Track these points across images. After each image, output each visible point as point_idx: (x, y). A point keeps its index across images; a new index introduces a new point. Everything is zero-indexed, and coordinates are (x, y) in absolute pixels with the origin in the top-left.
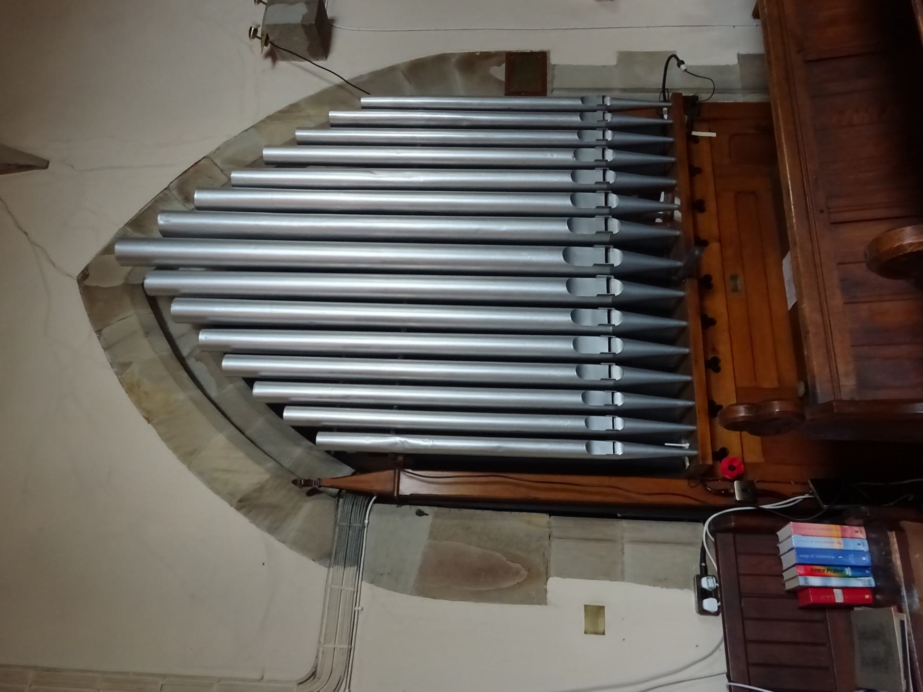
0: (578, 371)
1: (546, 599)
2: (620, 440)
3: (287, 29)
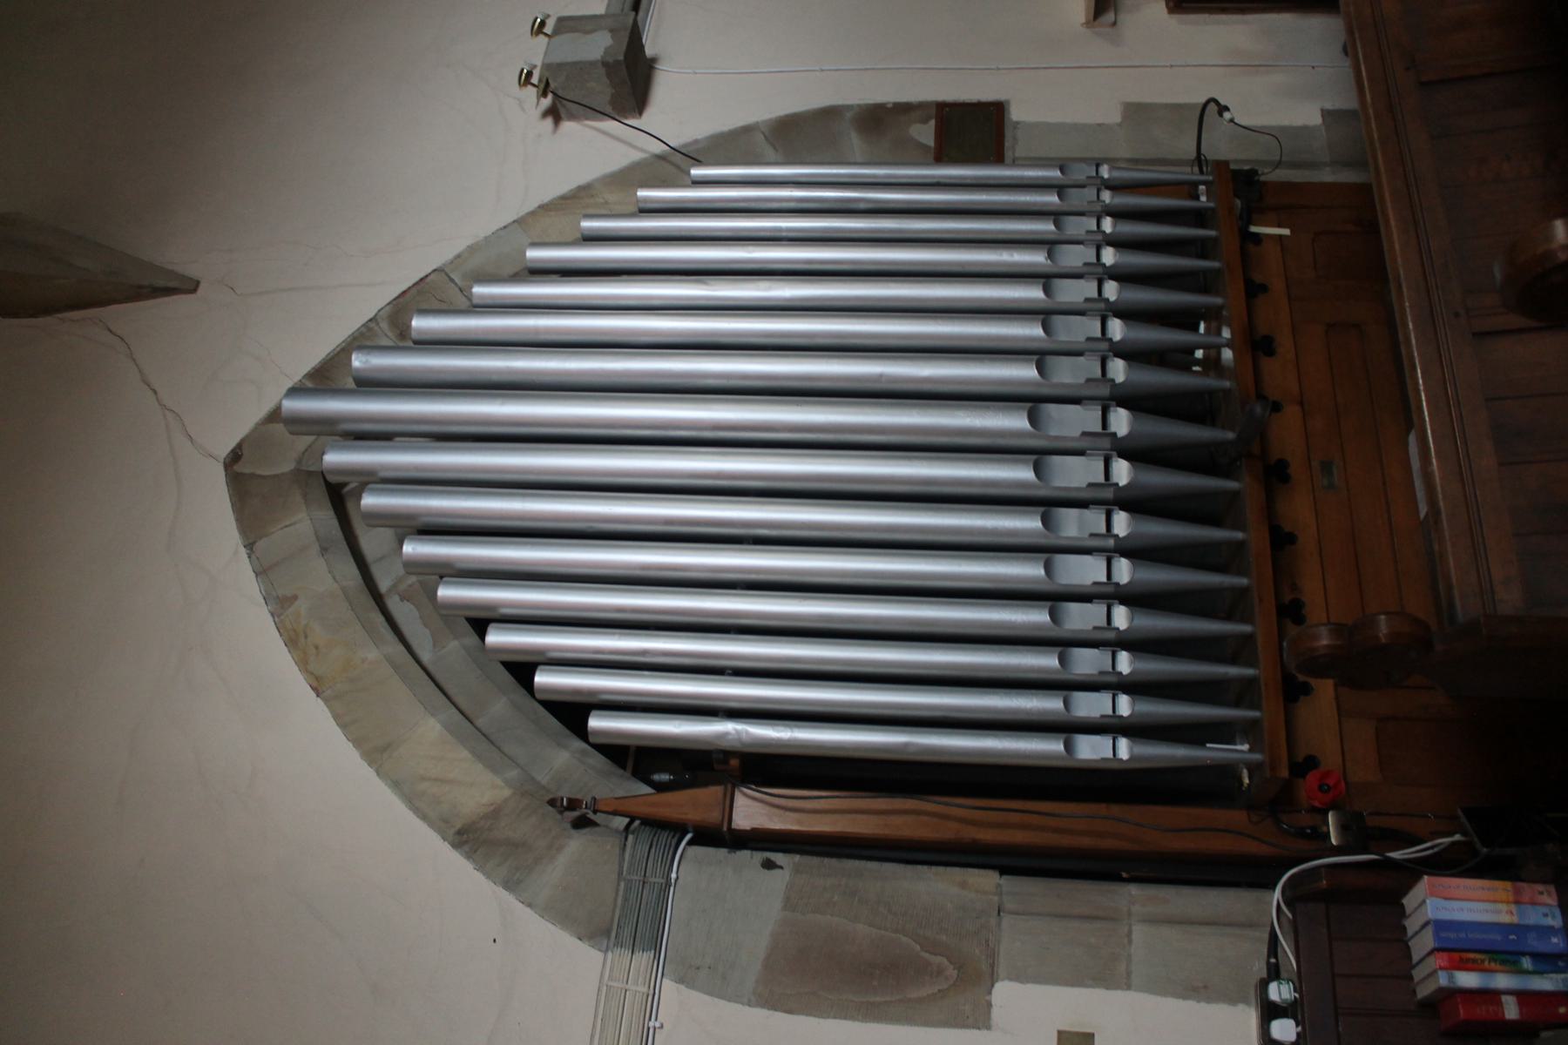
0: (1052, 614)
1: (989, 1018)
2: (1125, 735)
3: (578, 69)
